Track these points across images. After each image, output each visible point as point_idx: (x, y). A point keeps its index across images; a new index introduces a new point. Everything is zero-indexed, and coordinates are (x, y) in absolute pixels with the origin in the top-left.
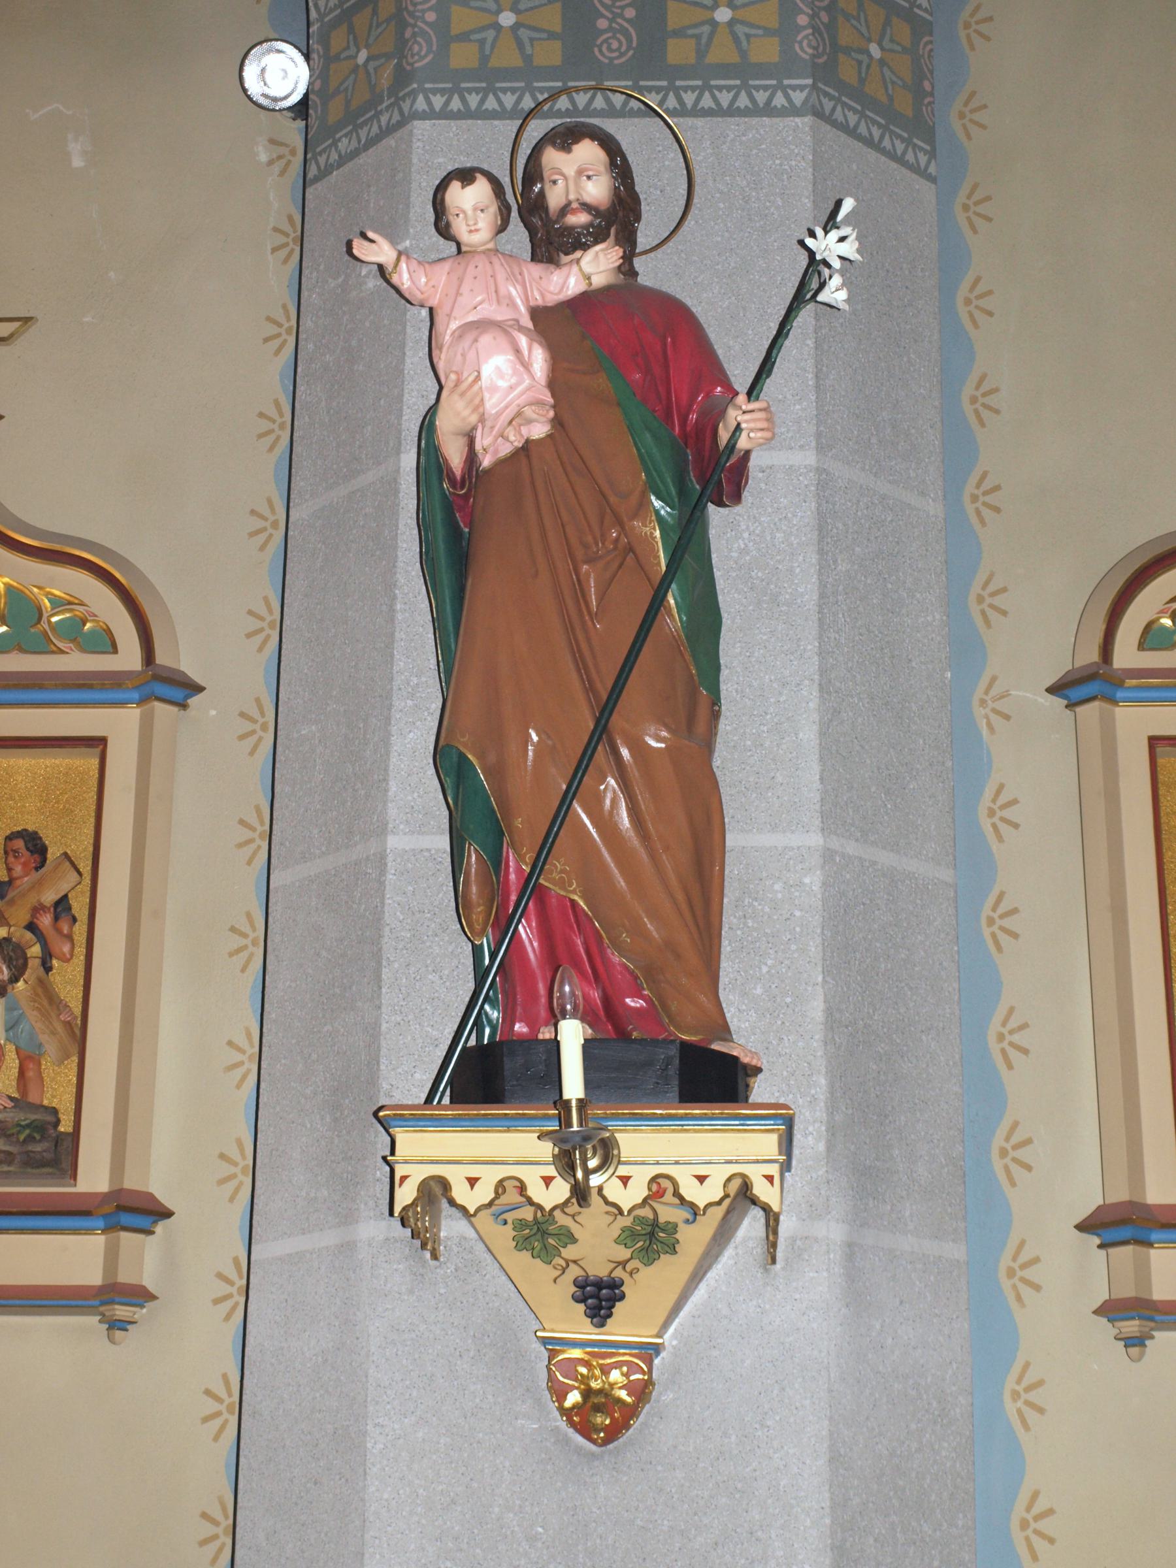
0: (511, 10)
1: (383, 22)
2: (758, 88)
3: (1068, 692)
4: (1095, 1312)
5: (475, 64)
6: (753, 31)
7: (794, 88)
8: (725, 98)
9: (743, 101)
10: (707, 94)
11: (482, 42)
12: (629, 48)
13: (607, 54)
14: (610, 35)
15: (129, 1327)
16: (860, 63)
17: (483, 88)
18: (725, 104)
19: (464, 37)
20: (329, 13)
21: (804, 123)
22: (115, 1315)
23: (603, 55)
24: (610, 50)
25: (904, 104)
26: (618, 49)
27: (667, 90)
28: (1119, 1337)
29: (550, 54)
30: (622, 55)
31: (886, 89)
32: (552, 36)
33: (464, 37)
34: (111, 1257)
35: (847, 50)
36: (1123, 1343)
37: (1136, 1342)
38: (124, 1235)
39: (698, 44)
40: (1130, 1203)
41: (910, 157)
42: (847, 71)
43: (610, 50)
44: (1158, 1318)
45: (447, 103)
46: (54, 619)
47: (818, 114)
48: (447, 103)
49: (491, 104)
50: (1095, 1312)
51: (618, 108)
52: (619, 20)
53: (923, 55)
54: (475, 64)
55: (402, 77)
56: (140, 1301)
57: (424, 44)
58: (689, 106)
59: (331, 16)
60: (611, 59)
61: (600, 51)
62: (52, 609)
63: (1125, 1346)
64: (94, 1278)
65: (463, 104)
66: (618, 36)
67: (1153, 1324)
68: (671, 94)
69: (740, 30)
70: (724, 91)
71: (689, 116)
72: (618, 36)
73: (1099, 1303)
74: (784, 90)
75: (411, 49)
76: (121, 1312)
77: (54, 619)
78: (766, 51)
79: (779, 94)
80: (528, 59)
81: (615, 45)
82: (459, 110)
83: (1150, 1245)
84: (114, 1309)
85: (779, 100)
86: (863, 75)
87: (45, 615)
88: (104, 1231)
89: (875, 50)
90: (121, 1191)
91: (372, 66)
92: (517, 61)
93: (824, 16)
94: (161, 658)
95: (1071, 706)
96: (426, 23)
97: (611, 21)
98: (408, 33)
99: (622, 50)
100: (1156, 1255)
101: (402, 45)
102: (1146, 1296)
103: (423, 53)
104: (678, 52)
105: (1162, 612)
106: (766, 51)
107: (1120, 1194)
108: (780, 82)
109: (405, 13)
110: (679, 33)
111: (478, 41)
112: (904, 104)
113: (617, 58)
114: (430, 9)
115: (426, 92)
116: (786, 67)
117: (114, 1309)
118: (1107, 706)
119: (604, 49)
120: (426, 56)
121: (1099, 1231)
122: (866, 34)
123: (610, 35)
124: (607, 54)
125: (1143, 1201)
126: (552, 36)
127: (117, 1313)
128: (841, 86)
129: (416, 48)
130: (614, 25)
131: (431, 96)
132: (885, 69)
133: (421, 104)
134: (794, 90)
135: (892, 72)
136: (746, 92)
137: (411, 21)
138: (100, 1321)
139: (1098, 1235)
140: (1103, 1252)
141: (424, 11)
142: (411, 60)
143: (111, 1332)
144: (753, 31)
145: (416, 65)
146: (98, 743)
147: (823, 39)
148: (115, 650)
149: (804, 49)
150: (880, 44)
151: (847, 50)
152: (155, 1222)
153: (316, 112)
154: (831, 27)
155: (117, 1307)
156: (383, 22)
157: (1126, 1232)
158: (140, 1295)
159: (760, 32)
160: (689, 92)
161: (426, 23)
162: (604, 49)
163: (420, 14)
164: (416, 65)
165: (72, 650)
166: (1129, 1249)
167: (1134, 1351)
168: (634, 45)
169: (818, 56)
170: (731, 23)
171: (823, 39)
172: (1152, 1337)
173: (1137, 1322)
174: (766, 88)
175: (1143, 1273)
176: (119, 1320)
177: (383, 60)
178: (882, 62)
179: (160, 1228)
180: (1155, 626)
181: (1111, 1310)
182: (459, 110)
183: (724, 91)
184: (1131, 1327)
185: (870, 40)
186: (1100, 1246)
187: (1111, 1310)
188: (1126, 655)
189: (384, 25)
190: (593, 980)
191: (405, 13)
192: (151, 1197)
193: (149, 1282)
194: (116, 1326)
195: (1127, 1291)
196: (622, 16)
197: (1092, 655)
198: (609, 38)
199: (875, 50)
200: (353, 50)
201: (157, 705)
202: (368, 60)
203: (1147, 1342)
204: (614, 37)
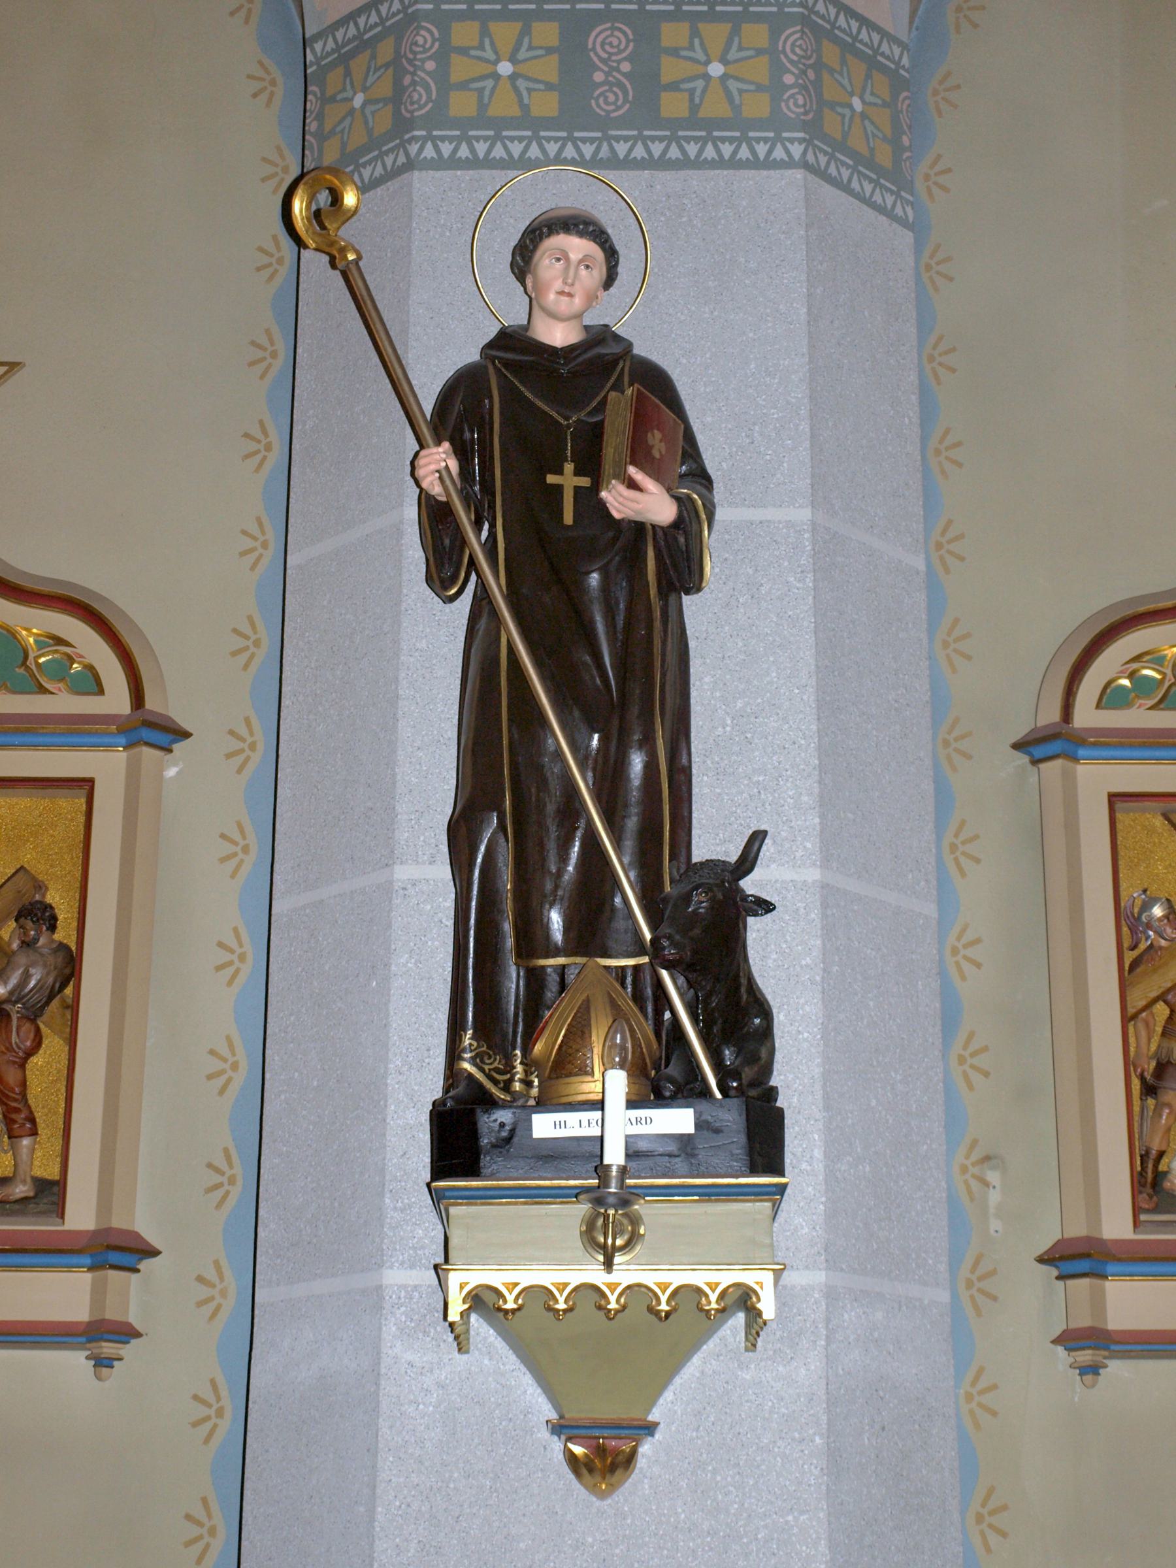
0: (509, 60)
1: (381, 67)
2: (548, 139)
3: (1031, 749)
4: (1053, 1342)
5: (686, 114)
6: (745, 87)
7: (584, 140)
8: (657, 149)
9: (464, 152)
10: (499, 144)
11: (481, 91)
12: (626, 101)
13: (794, 109)
14: (606, 88)
15: (116, 1363)
16: (843, 116)
17: (528, 137)
18: (727, 156)
19: (463, 86)
20: (326, 57)
21: (799, 175)
22: (102, 1353)
23: (599, 107)
24: (606, 102)
25: (884, 156)
26: (614, 103)
27: (635, 139)
28: (1076, 1365)
29: (546, 105)
30: (618, 108)
31: (868, 143)
32: (550, 87)
33: (463, 86)
34: (98, 1294)
35: (832, 105)
36: (1078, 1371)
37: (1092, 1370)
38: (112, 1273)
39: (692, 100)
40: (1089, 1239)
41: (899, 211)
42: (832, 124)
43: (606, 102)
44: (1113, 1347)
45: (455, 150)
46: (42, 660)
47: (806, 166)
48: (455, 150)
49: (710, 152)
50: (1053, 1342)
51: (692, 158)
52: (614, 73)
53: (901, 111)
54: (686, 114)
55: (402, 126)
56: (123, 1338)
57: (620, 93)
58: (727, 157)
59: (329, 59)
60: (609, 113)
61: (598, 106)
62: (38, 650)
63: (1080, 1374)
64: (81, 1314)
65: (752, 155)
66: (615, 89)
67: (1106, 1353)
68: (744, 145)
69: (733, 85)
70: (516, 142)
71: (483, 167)
72: (615, 89)
73: (1058, 1333)
74: (574, 141)
75: (410, 96)
76: (108, 1348)
77: (42, 660)
78: (757, 106)
79: (570, 145)
80: (525, 108)
81: (612, 98)
82: (747, 159)
83: (1104, 1277)
84: (101, 1347)
85: (744, 153)
86: (846, 129)
87: (31, 656)
88: (91, 1269)
89: (857, 104)
90: (109, 1230)
91: (369, 109)
92: (515, 111)
93: (811, 74)
94: (152, 703)
95: (1035, 762)
96: (602, 70)
97: (607, 74)
98: (407, 80)
99: (422, 102)
100: (1112, 1287)
101: (398, 95)
102: (1101, 1326)
103: (619, 103)
104: (673, 105)
105: (1122, 672)
106: (757, 106)
107: (1077, 1229)
108: (640, 133)
109: (404, 61)
110: (674, 87)
111: (476, 89)
112: (884, 156)
113: (614, 111)
114: (430, 58)
115: (434, 140)
116: (776, 123)
117: (101, 1347)
118: (1069, 764)
119: (601, 100)
120: (426, 104)
121: (1058, 1264)
122: (849, 89)
123: (606, 88)
124: (794, 109)
125: (1098, 1236)
126: (550, 87)
127: (105, 1350)
128: (825, 138)
129: (416, 97)
130: (610, 79)
131: (439, 143)
132: (867, 122)
133: (429, 152)
134: (549, 142)
135: (351, 124)
136: (467, 144)
137: (412, 69)
138: (87, 1358)
139: (1057, 1267)
140: (1061, 1284)
141: (423, 61)
142: (410, 108)
143: (98, 1369)
144: (745, 87)
145: (416, 114)
146: (86, 785)
147: (810, 96)
148: (101, 691)
149: (794, 106)
150: (862, 98)
151: (832, 105)
152: (141, 1259)
153: (313, 155)
154: (818, 83)
155: (104, 1344)
156: (381, 67)
157: (1083, 1265)
158: (126, 1333)
159: (542, 87)
160: (762, 143)
161: (602, 70)
162: (601, 100)
163: (615, 64)
164: (416, 114)
165: (60, 690)
166: (1085, 1281)
167: (1088, 1378)
168: (630, 98)
169: (806, 113)
170: (724, 78)
171: (810, 96)
172: (1106, 1366)
173: (1090, 1352)
174: (556, 139)
175: (1098, 1303)
176: (106, 1358)
177: (381, 105)
178: (863, 116)
179: (145, 1265)
180: (1137, 674)
181: (1069, 1339)
182: (747, 159)
183: (516, 142)
184: (1085, 1356)
185: (852, 94)
186: (1058, 1278)
187: (1069, 1339)
188: (1086, 715)
189: (382, 70)
190: (1159, 1029)
191: (404, 61)
192: (137, 1235)
193: (134, 1318)
194: (102, 1363)
195: (1083, 1321)
196: (618, 70)
197: (1051, 715)
198: (607, 91)
199: (857, 104)
200: (349, 94)
201: (146, 750)
202: (364, 105)
203: (1101, 1371)
204: (610, 90)
